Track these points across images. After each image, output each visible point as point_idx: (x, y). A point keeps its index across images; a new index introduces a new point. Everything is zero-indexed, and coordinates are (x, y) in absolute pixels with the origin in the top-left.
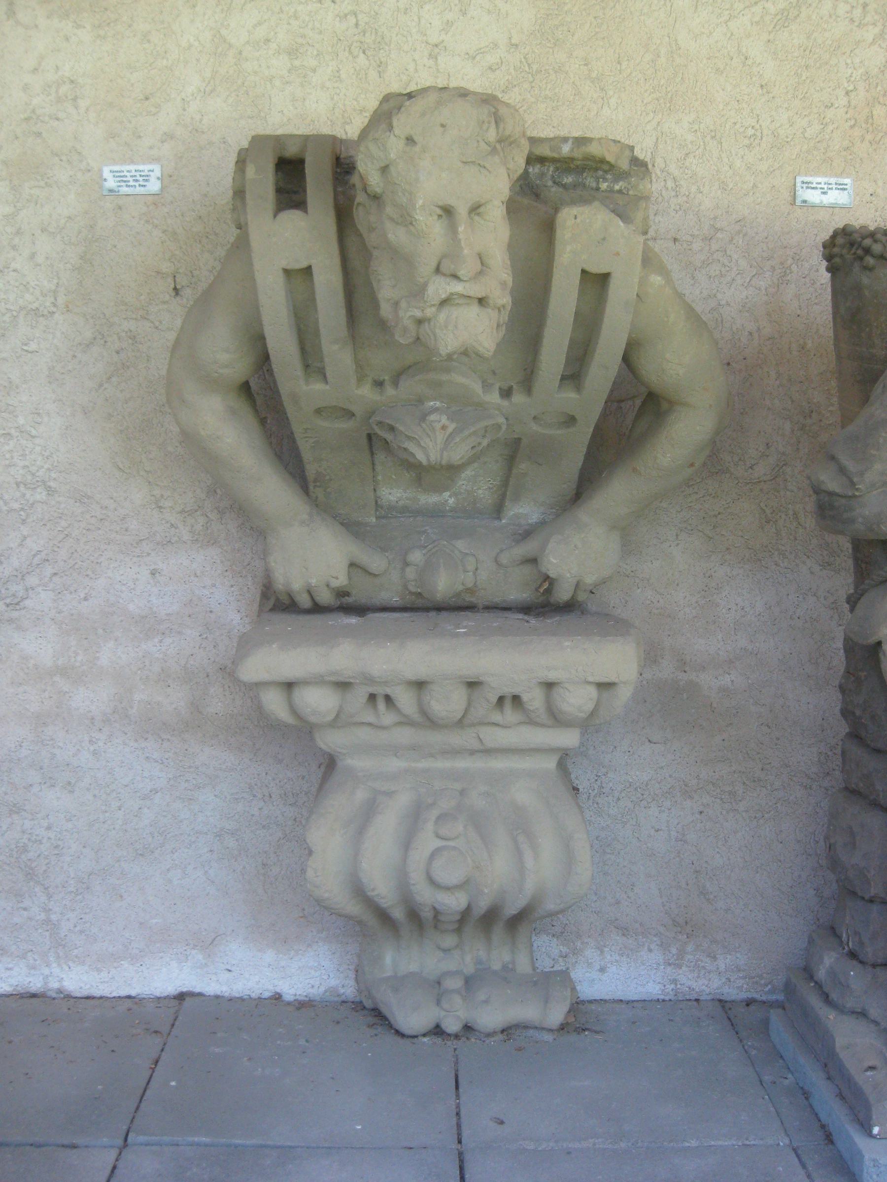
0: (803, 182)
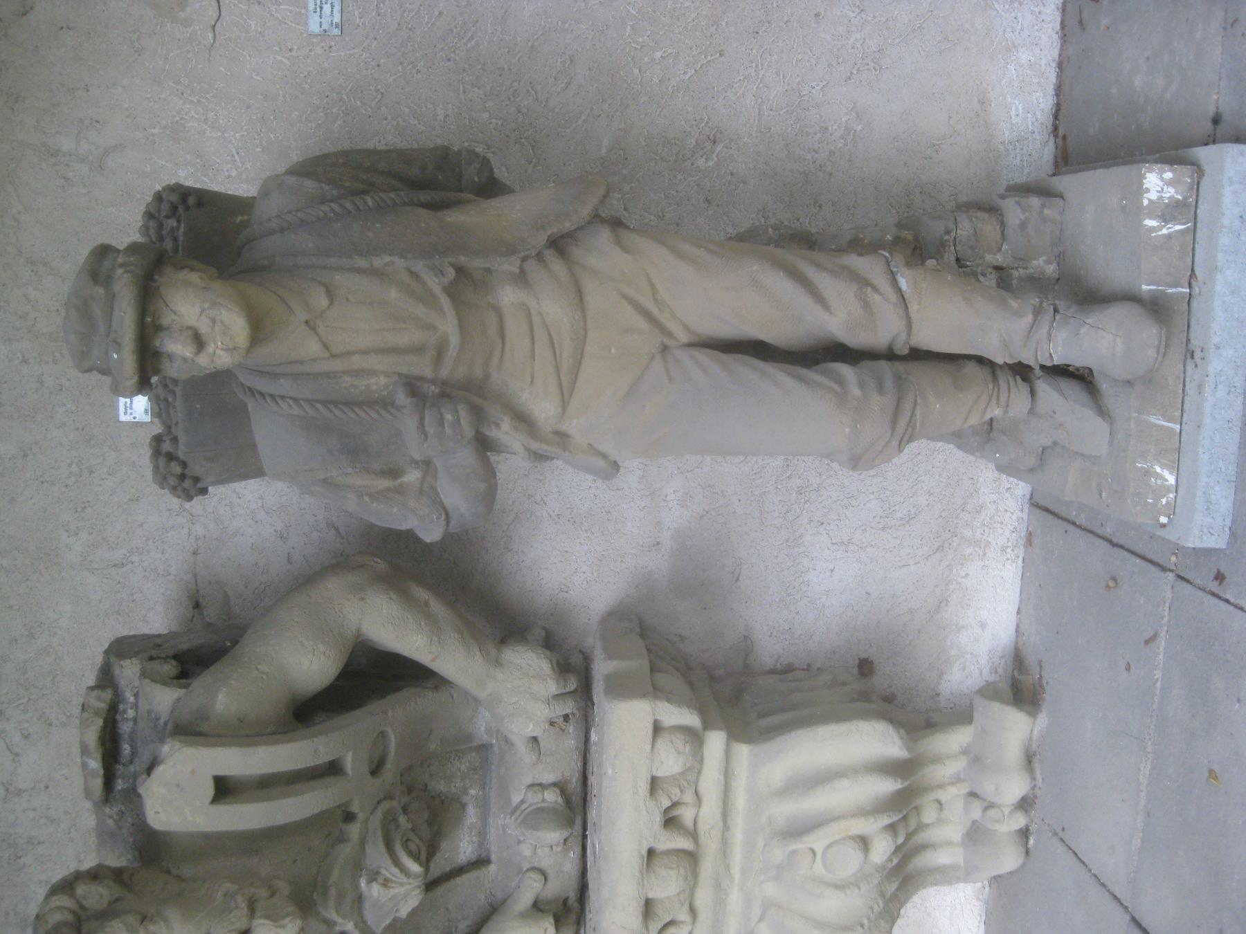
0: (125, 413)
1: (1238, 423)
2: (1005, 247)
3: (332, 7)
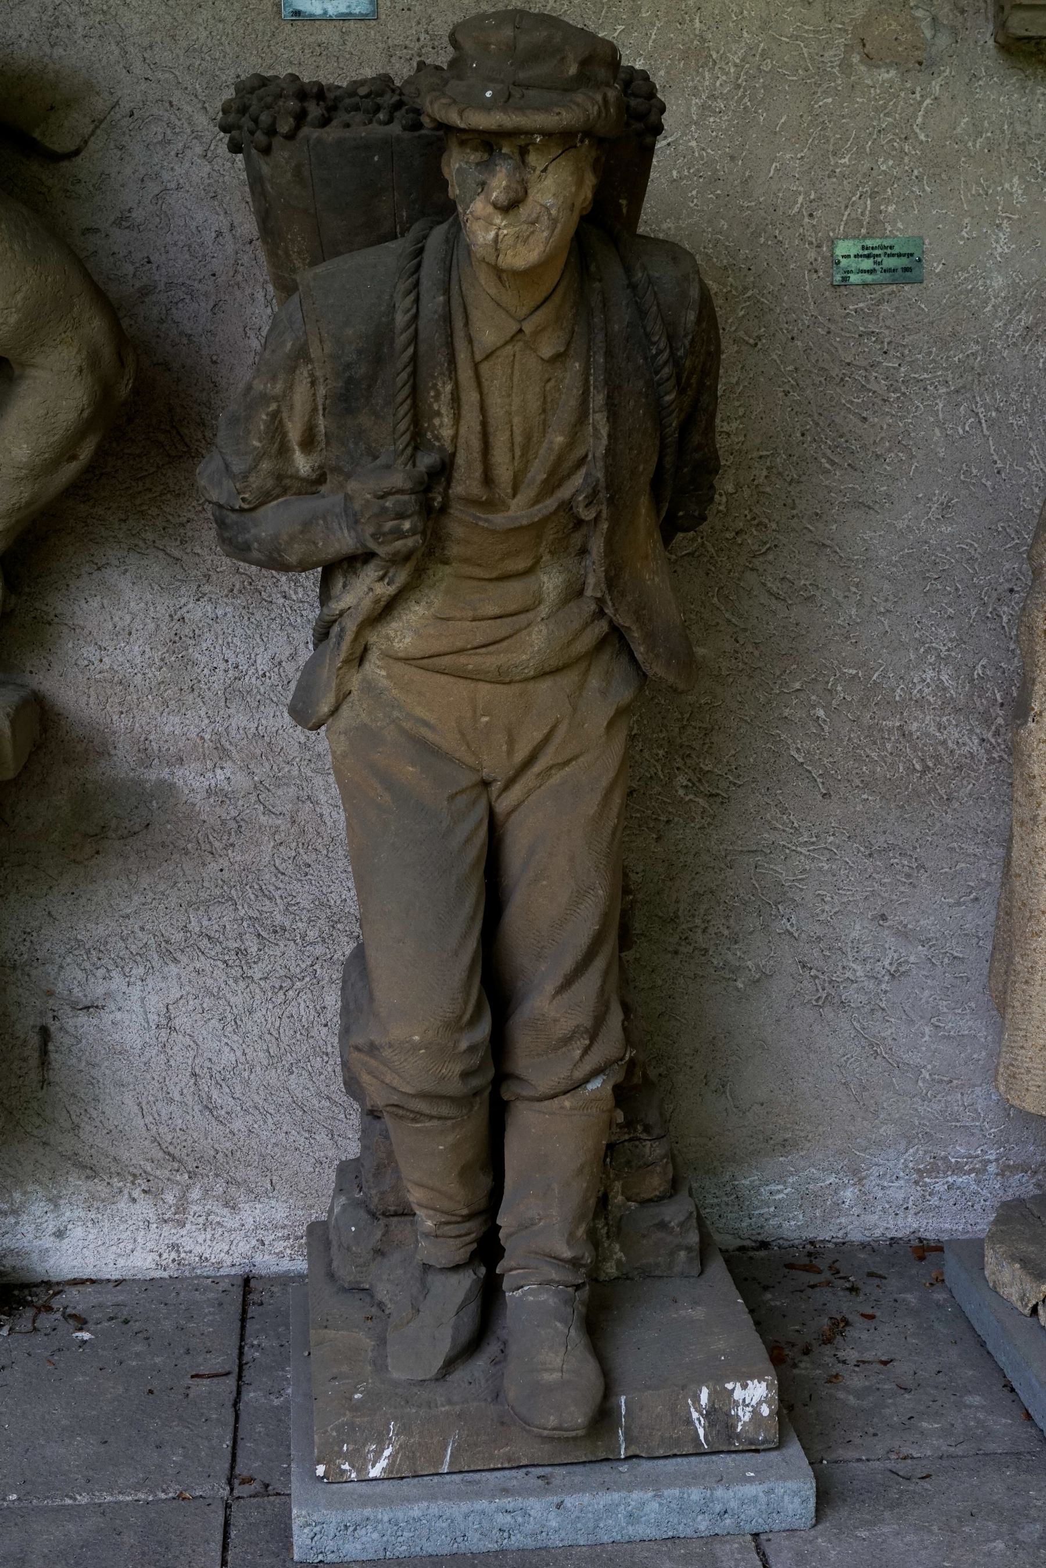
1: (463, 1547)
2: (633, 1205)
3: (871, 272)
